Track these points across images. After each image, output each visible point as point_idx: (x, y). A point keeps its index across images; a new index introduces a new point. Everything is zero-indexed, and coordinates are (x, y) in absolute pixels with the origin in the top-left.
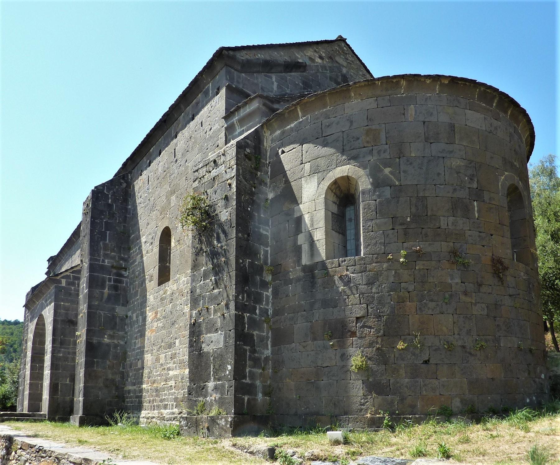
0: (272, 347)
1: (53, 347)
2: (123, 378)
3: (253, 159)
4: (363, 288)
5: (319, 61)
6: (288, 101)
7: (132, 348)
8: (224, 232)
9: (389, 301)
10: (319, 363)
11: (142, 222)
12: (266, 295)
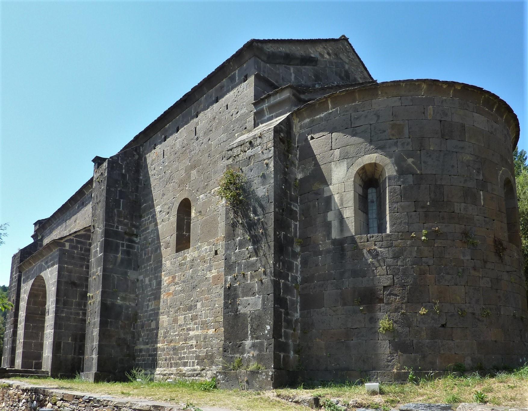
0: (300, 310)
1: (56, 307)
2: (133, 337)
3: (286, 142)
4: (389, 261)
5: (327, 56)
6: (311, 92)
7: (144, 310)
8: (262, 206)
9: (412, 272)
10: (349, 325)
11: (156, 193)
12: (296, 264)
